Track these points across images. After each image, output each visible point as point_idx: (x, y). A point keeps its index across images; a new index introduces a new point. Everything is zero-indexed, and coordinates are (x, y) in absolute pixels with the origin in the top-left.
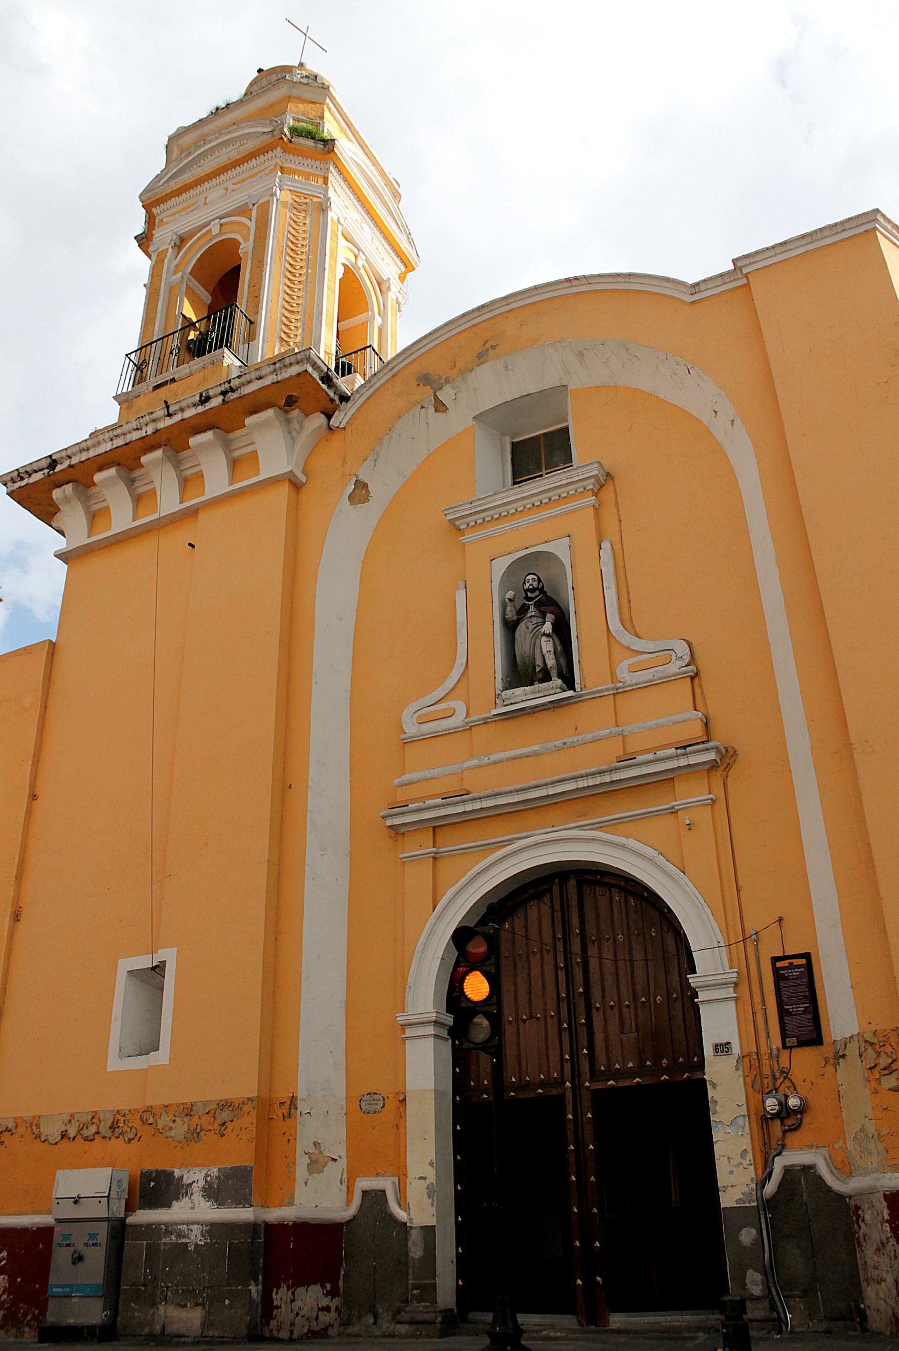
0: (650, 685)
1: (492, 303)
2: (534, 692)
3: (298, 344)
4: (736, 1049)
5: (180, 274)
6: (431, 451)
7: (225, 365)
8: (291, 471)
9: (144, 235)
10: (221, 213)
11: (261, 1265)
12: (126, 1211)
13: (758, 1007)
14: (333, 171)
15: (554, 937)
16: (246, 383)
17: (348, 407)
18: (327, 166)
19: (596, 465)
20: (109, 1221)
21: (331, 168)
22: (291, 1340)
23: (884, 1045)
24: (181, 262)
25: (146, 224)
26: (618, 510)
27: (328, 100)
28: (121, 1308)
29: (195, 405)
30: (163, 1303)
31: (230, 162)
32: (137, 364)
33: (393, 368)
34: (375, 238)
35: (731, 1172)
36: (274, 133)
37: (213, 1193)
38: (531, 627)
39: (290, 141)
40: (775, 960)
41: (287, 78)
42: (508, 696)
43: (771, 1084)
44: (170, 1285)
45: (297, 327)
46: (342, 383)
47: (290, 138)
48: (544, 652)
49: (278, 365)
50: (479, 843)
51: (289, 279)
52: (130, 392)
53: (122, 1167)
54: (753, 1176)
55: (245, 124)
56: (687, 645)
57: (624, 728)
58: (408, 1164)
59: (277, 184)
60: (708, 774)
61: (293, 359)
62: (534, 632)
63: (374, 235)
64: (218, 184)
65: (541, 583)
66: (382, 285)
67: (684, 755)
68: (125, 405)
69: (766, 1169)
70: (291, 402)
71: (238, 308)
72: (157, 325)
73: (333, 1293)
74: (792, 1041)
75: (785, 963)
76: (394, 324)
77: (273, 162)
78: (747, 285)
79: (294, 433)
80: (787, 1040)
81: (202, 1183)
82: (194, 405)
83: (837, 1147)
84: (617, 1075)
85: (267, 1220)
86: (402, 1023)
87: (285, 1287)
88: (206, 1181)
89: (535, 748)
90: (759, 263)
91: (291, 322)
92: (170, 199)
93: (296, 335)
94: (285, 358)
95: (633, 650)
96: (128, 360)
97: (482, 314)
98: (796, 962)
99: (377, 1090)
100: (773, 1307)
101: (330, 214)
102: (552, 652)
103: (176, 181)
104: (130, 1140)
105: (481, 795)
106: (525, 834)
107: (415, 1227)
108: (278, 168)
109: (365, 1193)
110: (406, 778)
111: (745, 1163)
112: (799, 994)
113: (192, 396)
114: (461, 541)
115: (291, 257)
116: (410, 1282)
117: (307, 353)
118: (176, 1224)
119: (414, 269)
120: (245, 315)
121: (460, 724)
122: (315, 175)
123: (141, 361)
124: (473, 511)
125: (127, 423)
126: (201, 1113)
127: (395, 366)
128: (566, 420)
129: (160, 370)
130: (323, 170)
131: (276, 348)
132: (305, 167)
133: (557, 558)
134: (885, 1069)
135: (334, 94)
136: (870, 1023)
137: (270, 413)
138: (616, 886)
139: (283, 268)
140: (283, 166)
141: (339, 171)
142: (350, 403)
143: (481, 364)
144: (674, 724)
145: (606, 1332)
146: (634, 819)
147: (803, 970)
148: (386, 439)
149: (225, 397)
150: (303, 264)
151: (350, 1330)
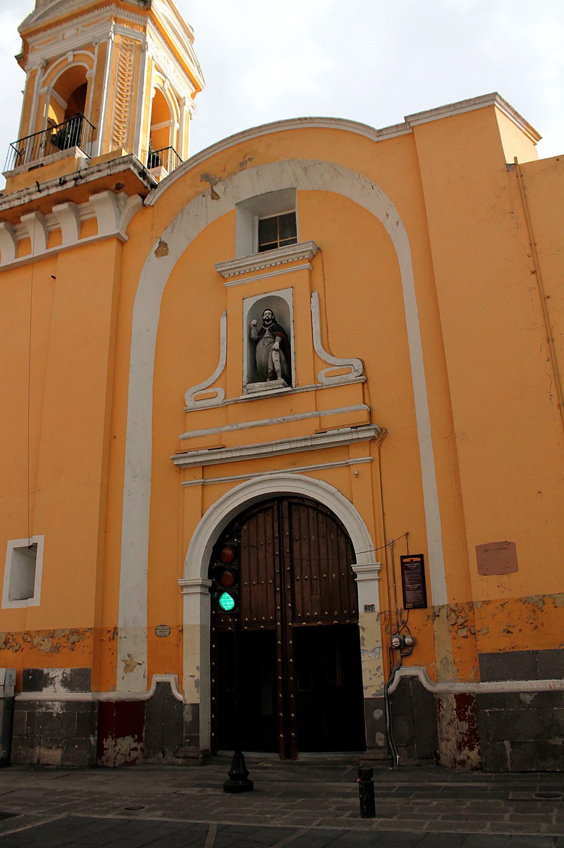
0: (338, 386)
2: (266, 386)
4: (377, 609)
5: (45, 89)
7: (76, 157)
8: (119, 233)
11: (97, 725)
12: (15, 692)
13: (391, 584)
14: (150, 23)
15: (274, 535)
18: (146, 19)
19: (311, 244)
20: (4, 699)
21: (149, 20)
22: (115, 768)
23: (461, 612)
26: (324, 273)
28: (12, 748)
29: (56, 186)
30: (38, 746)
32: (17, 150)
34: (176, 69)
35: (371, 679)
37: (68, 683)
38: (266, 344)
40: (403, 557)
42: (250, 388)
43: (396, 629)
44: (42, 736)
46: (151, 174)
48: (274, 361)
49: (111, 164)
50: (230, 478)
51: (119, 99)
52: (13, 171)
53: (12, 667)
54: (383, 681)
56: (361, 363)
57: (320, 412)
58: (184, 668)
60: (370, 443)
61: (121, 161)
62: (268, 348)
65: (274, 316)
66: (180, 101)
67: (356, 432)
69: (390, 677)
70: (119, 187)
73: (139, 740)
74: (409, 605)
75: (408, 560)
76: (187, 127)
77: (109, 14)
78: (412, 134)
79: (121, 208)
80: (407, 604)
81: (61, 677)
83: (431, 665)
84: (307, 619)
85: (100, 700)
86: (182, 584)
87: (111, 738)
88: (63, 676)
89: (266, 421)
90: (420, 121)
91: (120, 129)
94: (115, 159)
95: (328, 363)
96: (11, 147)
97: (244, 137)
98: (415, 559)
99: (166, 623)
100: (389, 752)
102: (279, 361)
104: (16, 651)
105: (232, 449)
106: (258, 474)
107: (187, 704)
109: (158, 684)
110: (187, 434)
111: (379, 674)
112: (415, 579)
113: (55, 180)
114: (225, 285)
115: (121, 83)
116: (184, 735)
117: (130, 157)
118: (45, 701)
119: (201, 90)
121: (221, 403)
122: (137, 25)
123: (20, 150)
124: (233, 267)
125: (12, 194)
126: (60, 636)
128: (294, 208)
129: (33, 158)
133: (284, 301)
134: (461, 625)
136: (454, 599)
137: (105, 194)
138: (312, 507)
139: (115, 91)
142: (157, 190)
143: (241, 170)
144: (351, 411)
145: (296, 764)
146: (324, 469)
147: (418, 564)
148: (180, 215)
149: (76, 182)
150: (129, 88)
151: (149, 760)
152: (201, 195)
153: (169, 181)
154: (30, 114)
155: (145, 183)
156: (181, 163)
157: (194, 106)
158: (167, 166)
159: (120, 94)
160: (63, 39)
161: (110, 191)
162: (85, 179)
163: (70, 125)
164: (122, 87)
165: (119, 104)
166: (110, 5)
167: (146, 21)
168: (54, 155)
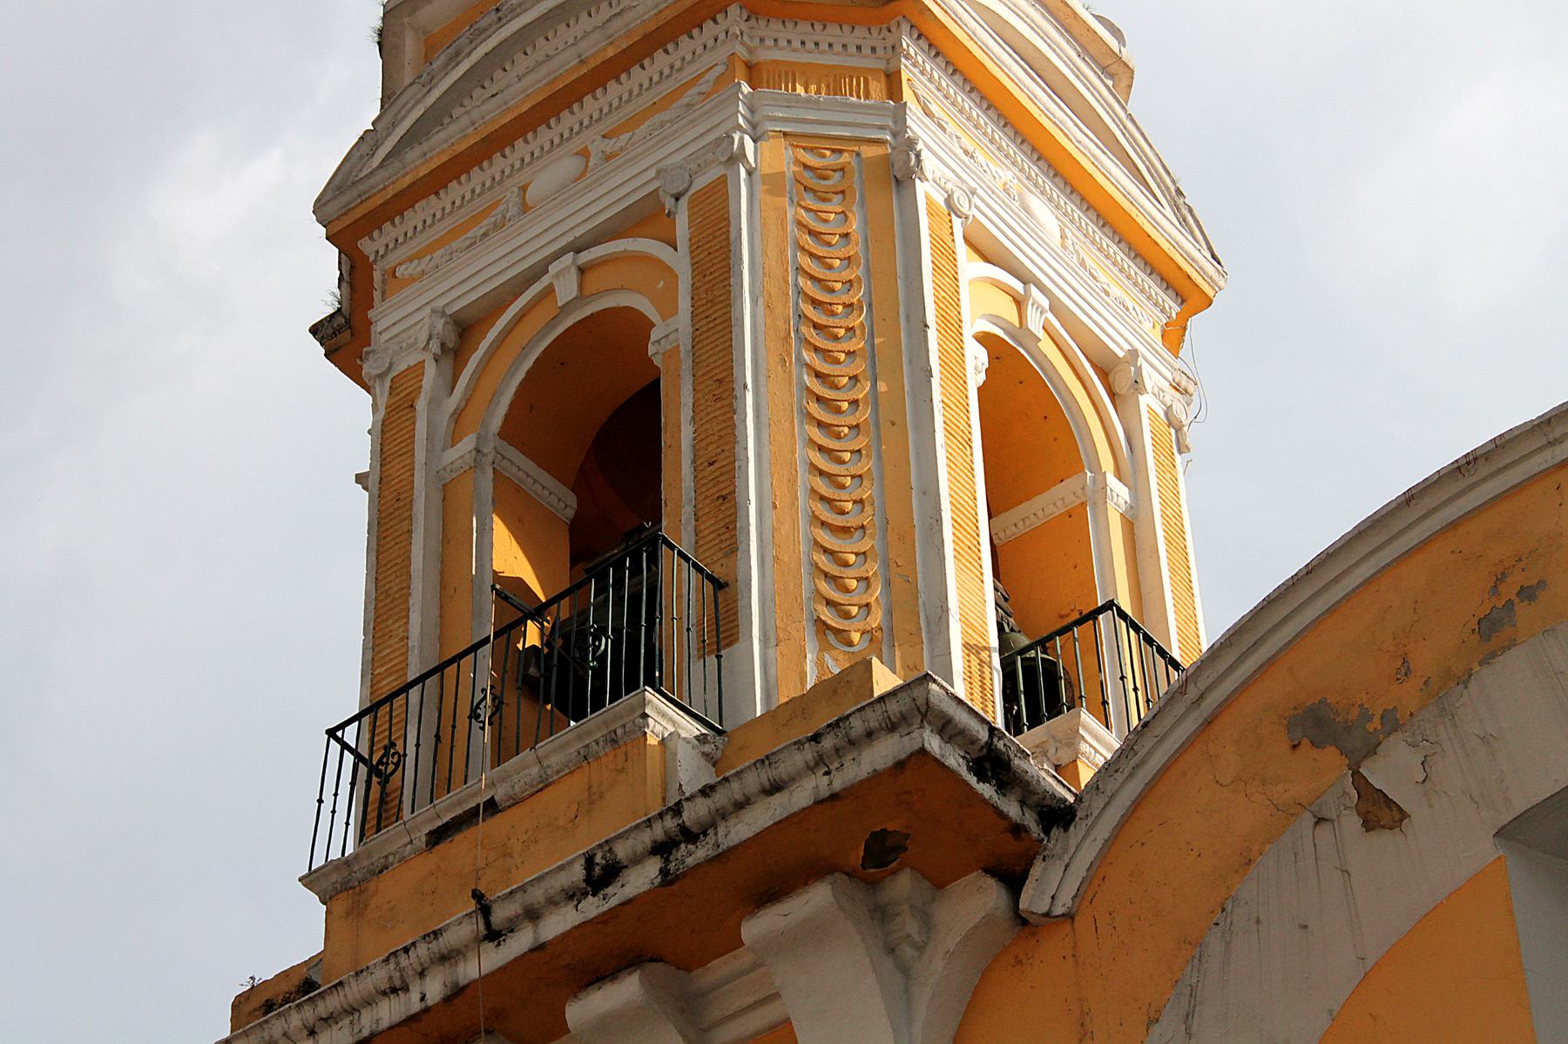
1: (1502, 444)
3: (878, 634)
5: (467, 444)
6: (1370, 963)
7: (652, 740)
9: (340, 320)
17: (1073, 843)
24: (467, 402)
25: (344, 285)
29: (573, 896)
31: (584, 70)
33: (1202, 697)
49: (828, 743)
51: (820, 424)
59: (741, 121)
61: (874, 718)
68: (341, 904)
71: (672, 547)
72: (415, 618)
77: (721, 54)
79: (908, 952)
82: (571, 897)
91: (846, 565)
92: (412, 206)
93: (868, 605)
96: (335, 747)
97: (1473, 486)
101: (921, 188)
108: (740, 71)
115: (816, 349)
117: (917, 692)
120: (695, 566)
122: (855, 72)
127: (1209, 688)
129: (441, 782)
130: (880, 52)
132: (823, 53)
137: (818, 897)
140: (754, 60)
142: (1077, 831)
143: (1494, 655)
149: (667, 861)
150: (859, 367)
152: (1307, 819)
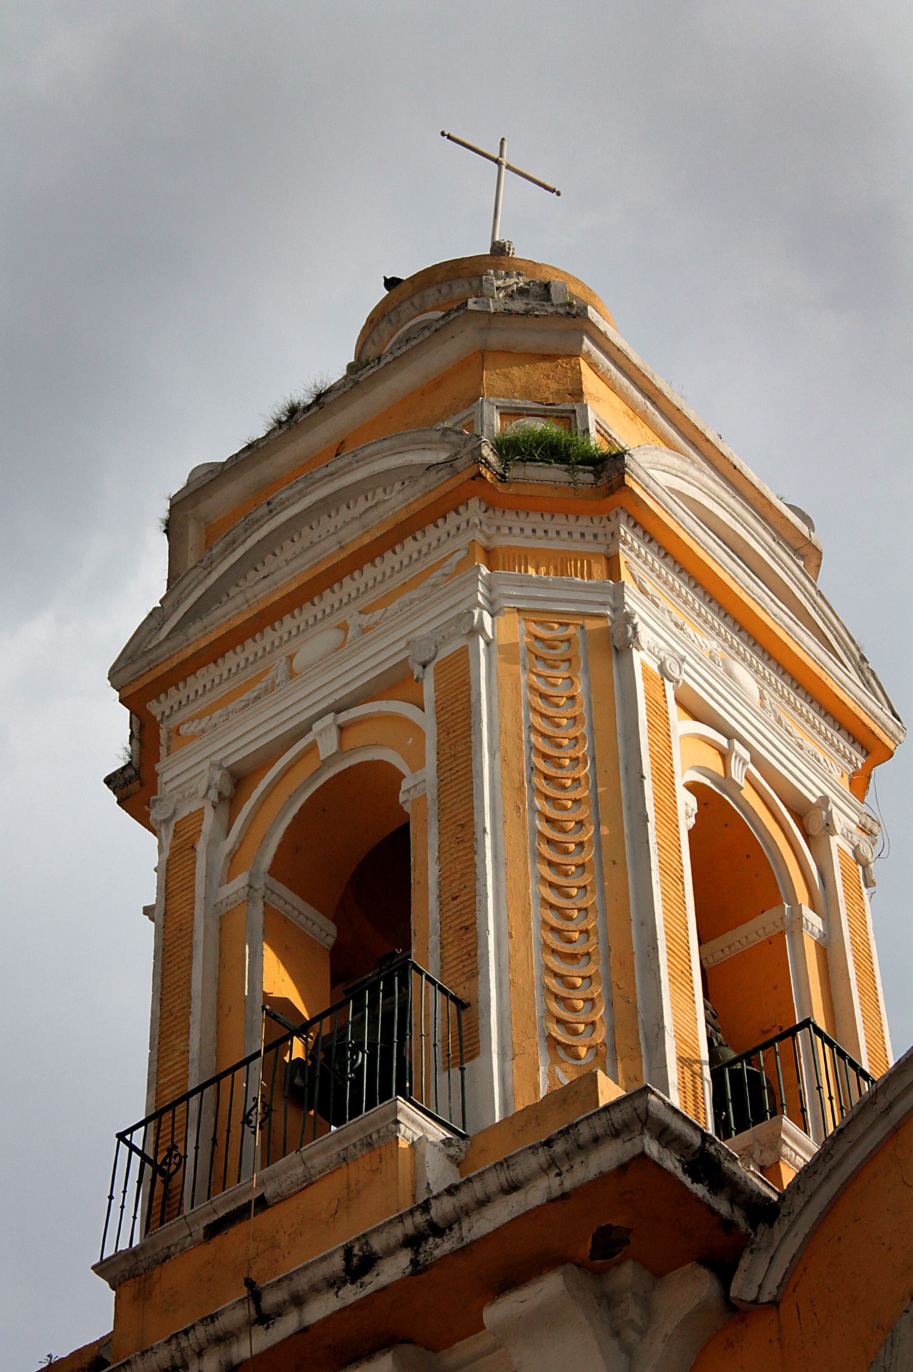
3: (602, 1049)
5: (240, 881)
7: (403, 1144)
10: (338, 696)
16: (473, 1206)
24: (241, 844)
25: (135, 741)
27: (587, 344)
29: (334, 1284)
31: (343, 555)
36: (458, 464)
39: (503, 478)
41: (471, 305)
45: (592, 999)
47: (501, 471)
49: (559, 1147)
51: (550, 864)
52: (141, 1247)
55: (374, 448)
59: (480, 598)
61: (599, 1125)
63: (765, 684)
64: (320, 616)
77: (462, 541)
79: (631, 1336)
91: (573, 987)
92: (194, 673)
96: (125, 1149)
101: (638, 657)
103: (206, 621)
108: (479, 555)
113: (324, 1259)
115: (547, 798)
117: (638, 1103)
119: (892, 755)
120: (441, 988)
122: (579, 556)
130: (601, 538)
131: (542, 1068)
135: (603, 326)
141: (645, 532)
142: (780, 1228)
149: (417, 1253)
150: (584, 813)
153: (828, 1177)
154: (189, 995)
155: (722, 1206)
156: (866, 1086)
157: (869, 824)
158: (803, 1110)
159: (549, 841)
160: (292, 675)
161: (570, 1268)
162: (456, 1233)
163: (358, 1009)
164: (554, 814)
165: (551, 885)
166: (462, 509)
167: (614, 535)
168: (309, 1149)
